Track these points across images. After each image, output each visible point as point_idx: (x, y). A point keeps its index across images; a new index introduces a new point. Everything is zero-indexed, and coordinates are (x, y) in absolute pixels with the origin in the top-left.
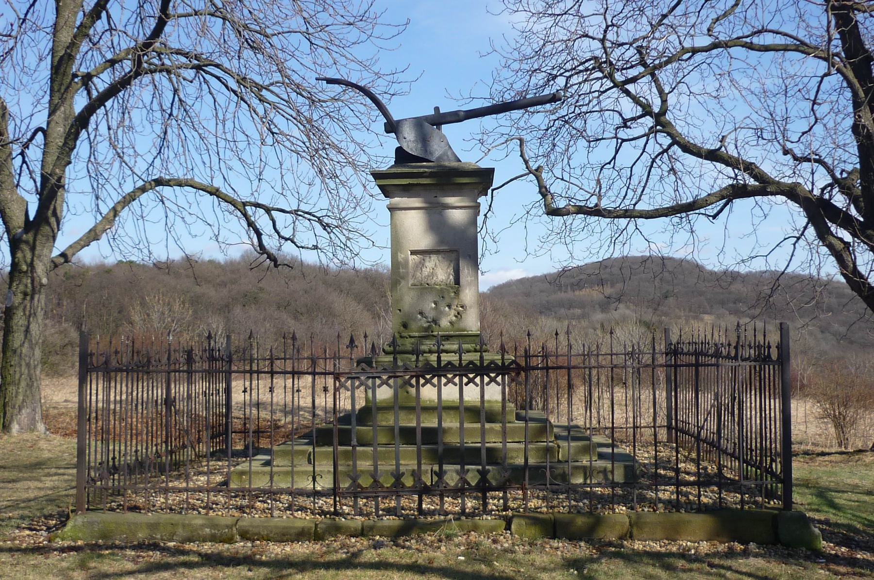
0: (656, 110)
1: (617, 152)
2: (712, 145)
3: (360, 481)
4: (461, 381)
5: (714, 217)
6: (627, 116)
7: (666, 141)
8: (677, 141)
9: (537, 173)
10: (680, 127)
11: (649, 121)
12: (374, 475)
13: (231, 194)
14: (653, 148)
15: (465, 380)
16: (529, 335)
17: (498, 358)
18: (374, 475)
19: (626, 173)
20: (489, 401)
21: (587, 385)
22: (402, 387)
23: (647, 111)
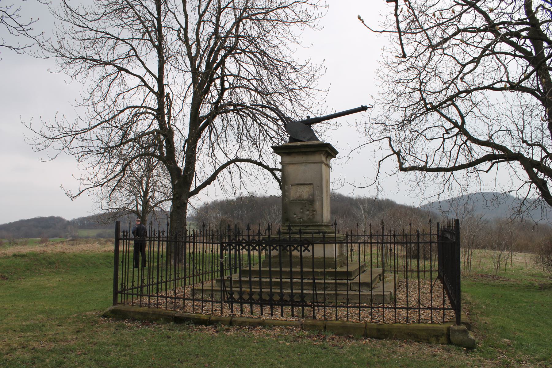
0: (460, 124)
1: (10, 47)
2: (485, 138)
3: (253, 297)
4: (270, 248)
5: (487, 172)
6: (447, 128)
7: (464, 138)
8: (470, 138)
9: (398, 154)
10: (471, 131)
11: (456, 130)
12: (261, 293)
13: (265, 164)
14: (459, 142)
15: (272, 248)
16: (370, 225)
17: (246, 238)
18: (261, 293)
19: (448, 154)
20: (328, 258)
21: (252, 257)
22: (283, 250)
23: (456, 125)
